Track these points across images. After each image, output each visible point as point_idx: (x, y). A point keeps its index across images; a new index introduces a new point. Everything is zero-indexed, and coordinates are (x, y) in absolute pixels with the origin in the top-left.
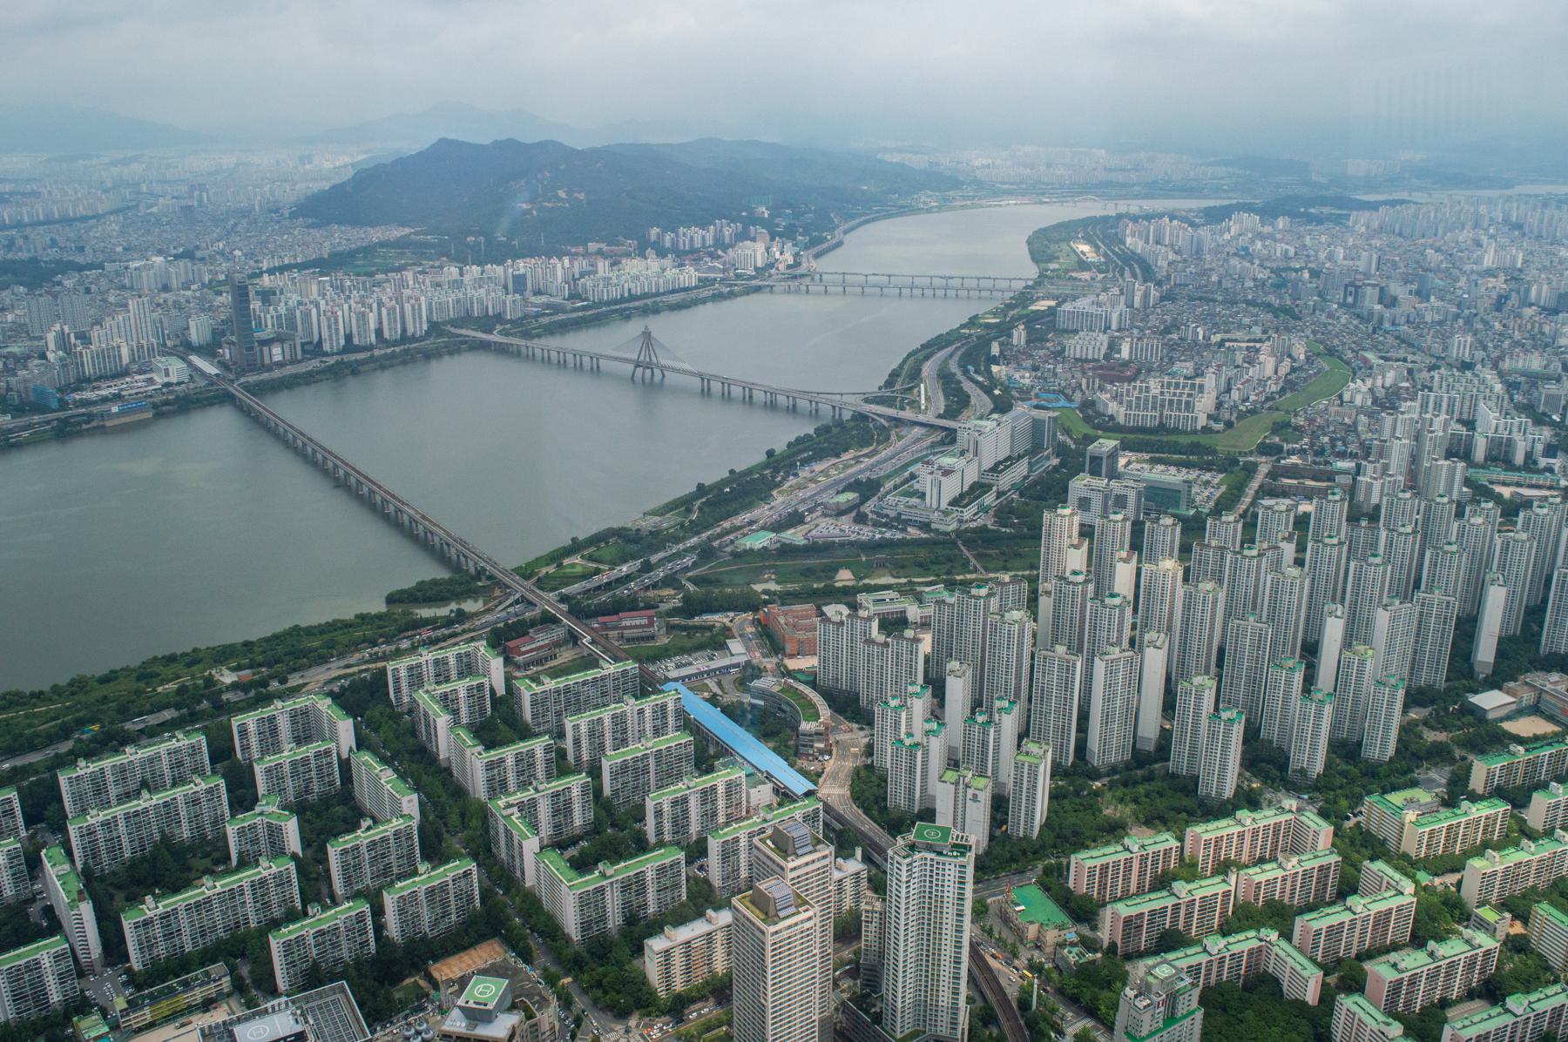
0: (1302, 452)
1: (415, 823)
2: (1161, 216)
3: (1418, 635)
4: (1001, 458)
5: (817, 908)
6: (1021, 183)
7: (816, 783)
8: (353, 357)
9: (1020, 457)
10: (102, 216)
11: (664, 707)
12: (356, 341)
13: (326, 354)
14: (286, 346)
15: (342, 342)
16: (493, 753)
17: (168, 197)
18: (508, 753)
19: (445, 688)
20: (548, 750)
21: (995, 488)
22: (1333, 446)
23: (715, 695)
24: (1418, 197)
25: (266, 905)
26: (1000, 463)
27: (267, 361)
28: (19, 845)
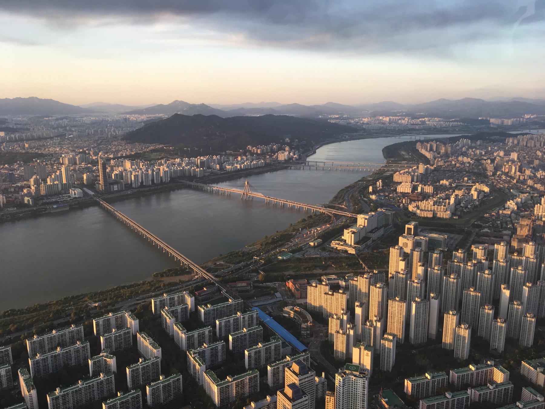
0: (489, 227)
1: (159, 360)
2: (432, 140)
3: (540, 298)
4: (373, 228)
5: (309, 396)
6: (380, 130)
7: (307, 346)
8: (143, 189)
9: (381, 228)
10: (53, 138)
11: (252, 316)
12: (144, 184)
13: (133, 188)
14: (119, 185)
15: (139, 184)
16: (189, 333)
17: (77, 131)
18: (196, 333)
19: (173, 309)
20: (210, 332)
21: (371, 239)
22: (502, 225)
23: (270, 312)
24: (533, 131)
25: (102, 392)
26: (373, 230)
27: (112, 190)
28: (10, 368)
